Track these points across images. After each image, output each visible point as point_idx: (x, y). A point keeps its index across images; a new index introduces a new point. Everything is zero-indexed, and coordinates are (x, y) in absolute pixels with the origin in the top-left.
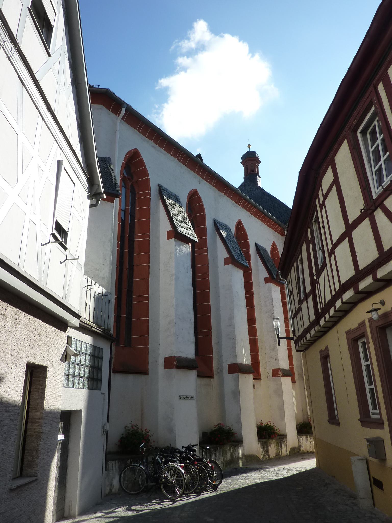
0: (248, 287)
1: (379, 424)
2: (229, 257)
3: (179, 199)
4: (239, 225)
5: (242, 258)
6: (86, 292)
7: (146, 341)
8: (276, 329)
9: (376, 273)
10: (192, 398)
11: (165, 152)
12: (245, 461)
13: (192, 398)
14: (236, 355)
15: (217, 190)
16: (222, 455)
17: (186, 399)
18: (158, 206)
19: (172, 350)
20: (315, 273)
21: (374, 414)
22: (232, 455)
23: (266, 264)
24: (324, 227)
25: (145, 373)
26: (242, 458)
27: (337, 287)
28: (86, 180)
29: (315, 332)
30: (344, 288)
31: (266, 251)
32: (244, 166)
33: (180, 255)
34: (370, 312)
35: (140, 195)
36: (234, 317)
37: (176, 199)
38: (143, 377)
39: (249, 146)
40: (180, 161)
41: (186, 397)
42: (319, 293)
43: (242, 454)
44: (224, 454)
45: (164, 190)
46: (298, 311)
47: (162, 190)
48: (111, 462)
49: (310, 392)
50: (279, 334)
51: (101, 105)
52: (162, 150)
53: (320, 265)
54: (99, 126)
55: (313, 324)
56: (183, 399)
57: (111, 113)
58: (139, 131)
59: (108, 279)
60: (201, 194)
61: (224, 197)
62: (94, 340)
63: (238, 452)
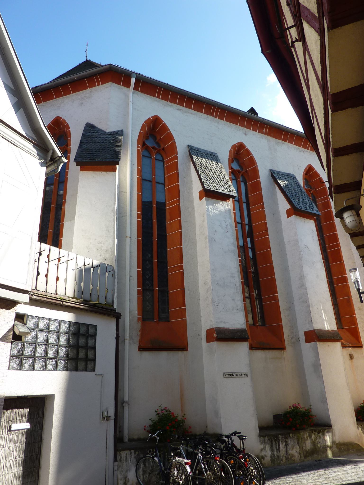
2: (290, 207)
6: (58, 265)
7: (183, 313)
8: (354, 282)
10: (243, 375)
12: (338, 451)
13: (243, 375)
14: (311, 321)
15: (272, 138)
16: (297, 443)
17: (234, 376)
18: (189, 169)
19: (211, 321)
22: (314, 443)
25: (184, 348)
26: (331, 447)
28: (33, 146)
33: (214, 214)
36: (304, 276)
37: (213, 157)
38: (180, 354)
40: (216, 117)
41: (235, 375)
43: (331, 442)
44: (300, 442)
48: (125, 451)
50: (360, 289)
51: (110, 83)
52: (191, 111)
54: (109, 103)
56: (229, 376)
57: (123, 87)
58: (158, 97)
59: (112, 251)
61: (283, 144)
62: (77, 317)
63: (324, 439)
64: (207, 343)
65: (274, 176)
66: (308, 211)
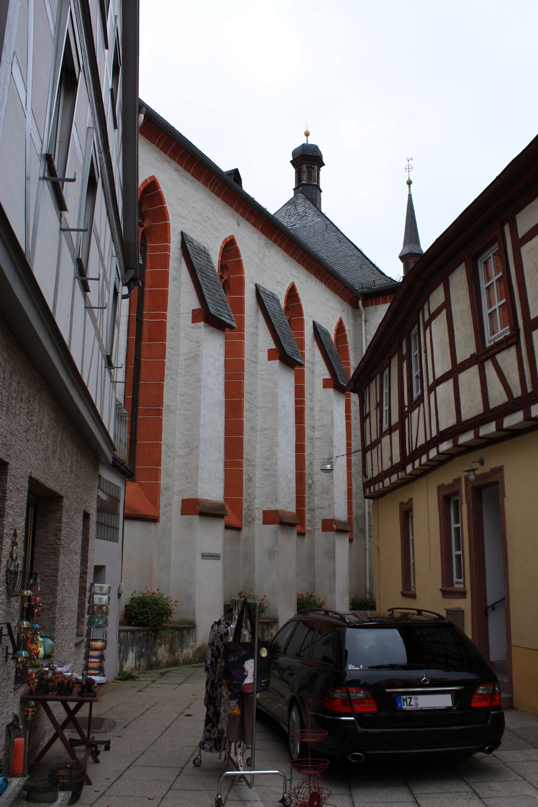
0: (300, 392)
1: (462, 594)
2: (200, 307)
3: (209, 255)
4: (292, 293)
5: (295, 351)
9: (479, 430)
11: (191, 178)
14: (276, 499)
20: (406, 403)
21: (457, 583)
23: (328, 357)
24: (426, 352)
27: (434, 434)
29: (398, 479)
30: (443, 436)
31: (328, 335)
32: (295, 168)
34: (468, 471)
35: (153, 249)
39: (307, 134)
42: (409, 439)
45: (190, 242)
46: (376, 443)
47: (187, 242)
49: (379, 555)
53: (415, 395)
55: (395, 469)
60: (239, 244)
64: (182, 516)
65: (186, 246)
66: (294, 357)
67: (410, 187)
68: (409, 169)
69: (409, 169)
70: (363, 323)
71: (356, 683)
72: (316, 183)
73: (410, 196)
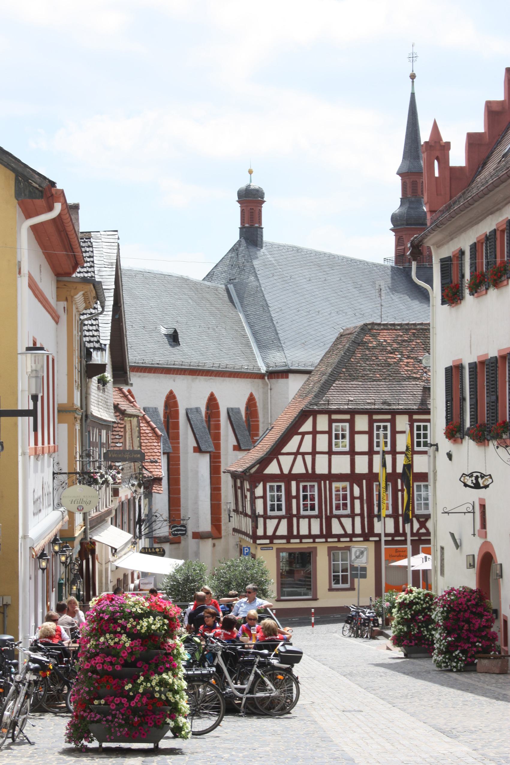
67: (413, 82)
68: (413, 58)
69: (413, 58)
70: (269, 391)
71: (152, 630)
72: (64, 705)
73: (413, 95)
